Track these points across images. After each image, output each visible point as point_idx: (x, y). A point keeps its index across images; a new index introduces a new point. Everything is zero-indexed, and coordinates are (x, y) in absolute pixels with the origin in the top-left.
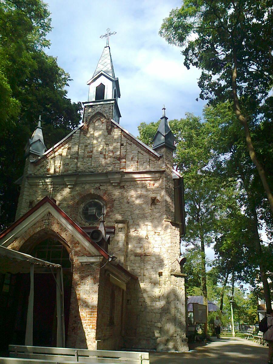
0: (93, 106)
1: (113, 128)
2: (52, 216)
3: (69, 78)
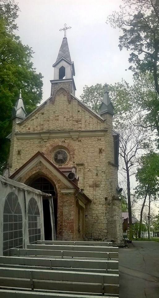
0: (58, 84)
3: (32, 52)
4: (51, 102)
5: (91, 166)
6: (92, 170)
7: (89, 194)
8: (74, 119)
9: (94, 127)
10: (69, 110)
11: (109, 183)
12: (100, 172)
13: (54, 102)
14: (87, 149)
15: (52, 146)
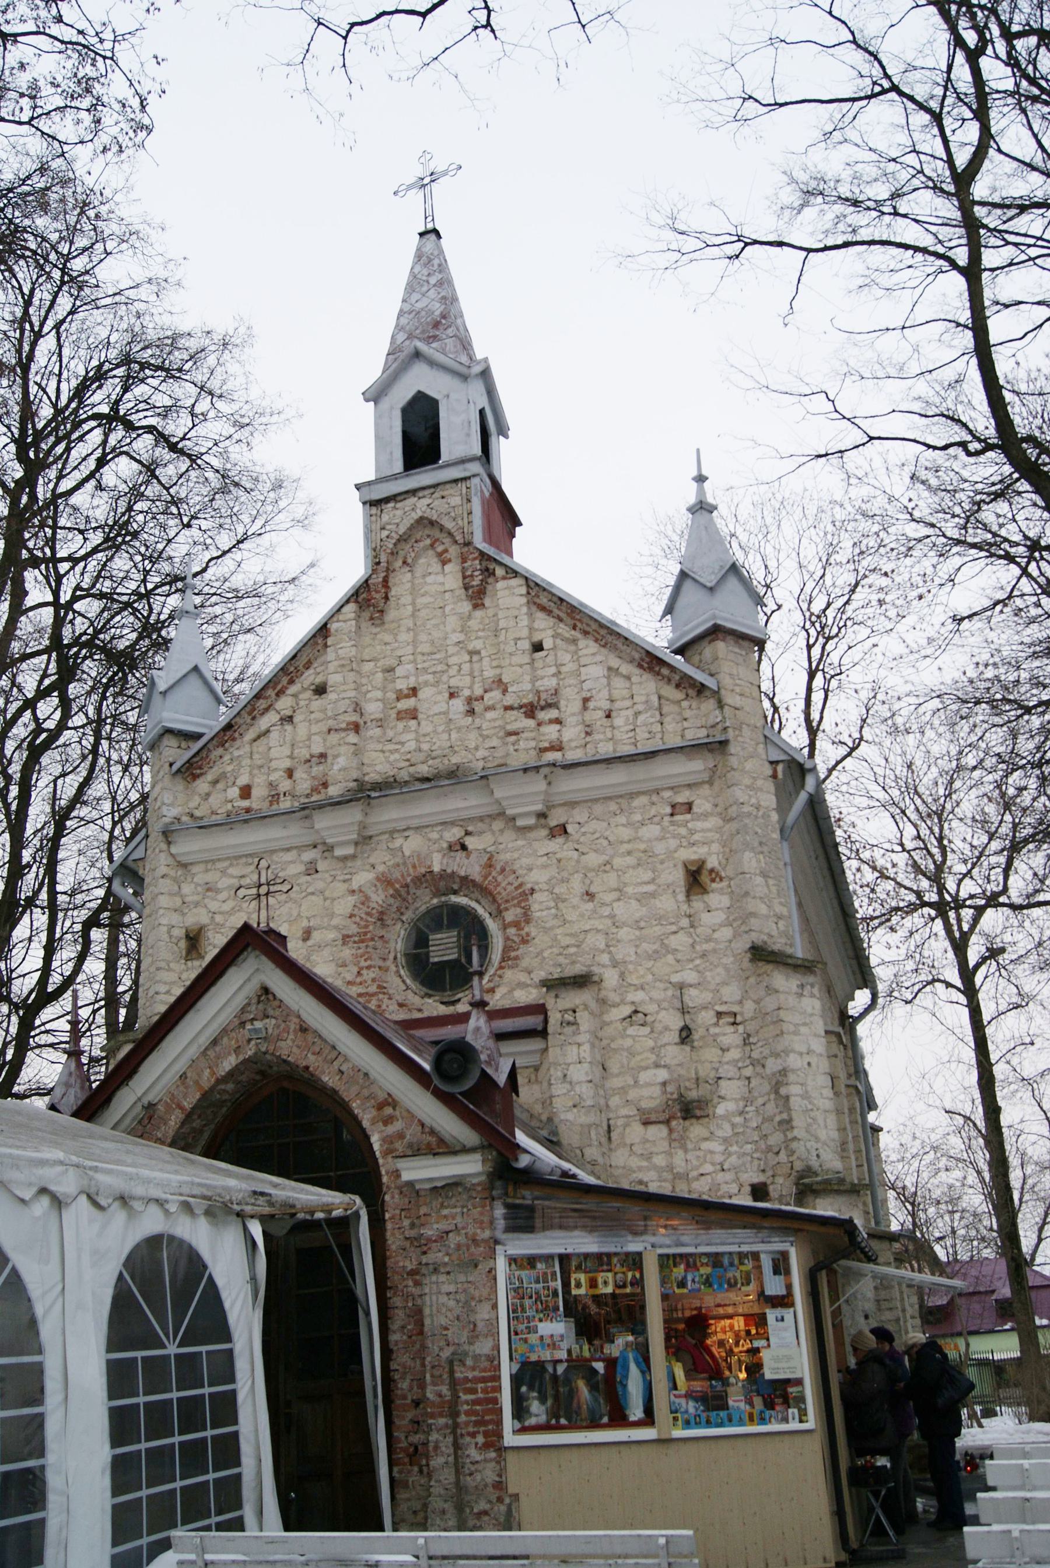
1: (491, 580)
2: (277, 1003)
4: (366, 615)
5: (643, 988)
6: (651, 1008)
7: (640, 1169)
8: (509, 700)
9: (642, 734)
10: (477, 645)
11: (766, 1087)
12: (707, 1017)
13: (382, 611)
14: (612, 879)
15: (385, 881)
